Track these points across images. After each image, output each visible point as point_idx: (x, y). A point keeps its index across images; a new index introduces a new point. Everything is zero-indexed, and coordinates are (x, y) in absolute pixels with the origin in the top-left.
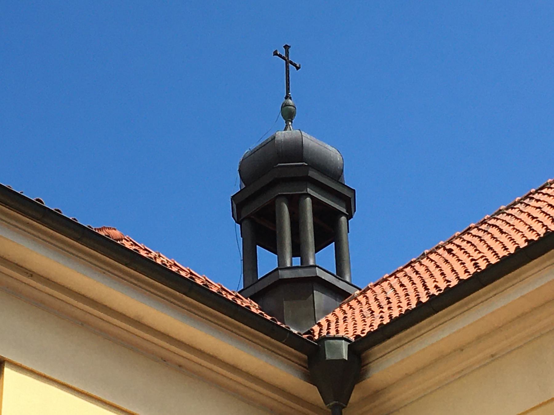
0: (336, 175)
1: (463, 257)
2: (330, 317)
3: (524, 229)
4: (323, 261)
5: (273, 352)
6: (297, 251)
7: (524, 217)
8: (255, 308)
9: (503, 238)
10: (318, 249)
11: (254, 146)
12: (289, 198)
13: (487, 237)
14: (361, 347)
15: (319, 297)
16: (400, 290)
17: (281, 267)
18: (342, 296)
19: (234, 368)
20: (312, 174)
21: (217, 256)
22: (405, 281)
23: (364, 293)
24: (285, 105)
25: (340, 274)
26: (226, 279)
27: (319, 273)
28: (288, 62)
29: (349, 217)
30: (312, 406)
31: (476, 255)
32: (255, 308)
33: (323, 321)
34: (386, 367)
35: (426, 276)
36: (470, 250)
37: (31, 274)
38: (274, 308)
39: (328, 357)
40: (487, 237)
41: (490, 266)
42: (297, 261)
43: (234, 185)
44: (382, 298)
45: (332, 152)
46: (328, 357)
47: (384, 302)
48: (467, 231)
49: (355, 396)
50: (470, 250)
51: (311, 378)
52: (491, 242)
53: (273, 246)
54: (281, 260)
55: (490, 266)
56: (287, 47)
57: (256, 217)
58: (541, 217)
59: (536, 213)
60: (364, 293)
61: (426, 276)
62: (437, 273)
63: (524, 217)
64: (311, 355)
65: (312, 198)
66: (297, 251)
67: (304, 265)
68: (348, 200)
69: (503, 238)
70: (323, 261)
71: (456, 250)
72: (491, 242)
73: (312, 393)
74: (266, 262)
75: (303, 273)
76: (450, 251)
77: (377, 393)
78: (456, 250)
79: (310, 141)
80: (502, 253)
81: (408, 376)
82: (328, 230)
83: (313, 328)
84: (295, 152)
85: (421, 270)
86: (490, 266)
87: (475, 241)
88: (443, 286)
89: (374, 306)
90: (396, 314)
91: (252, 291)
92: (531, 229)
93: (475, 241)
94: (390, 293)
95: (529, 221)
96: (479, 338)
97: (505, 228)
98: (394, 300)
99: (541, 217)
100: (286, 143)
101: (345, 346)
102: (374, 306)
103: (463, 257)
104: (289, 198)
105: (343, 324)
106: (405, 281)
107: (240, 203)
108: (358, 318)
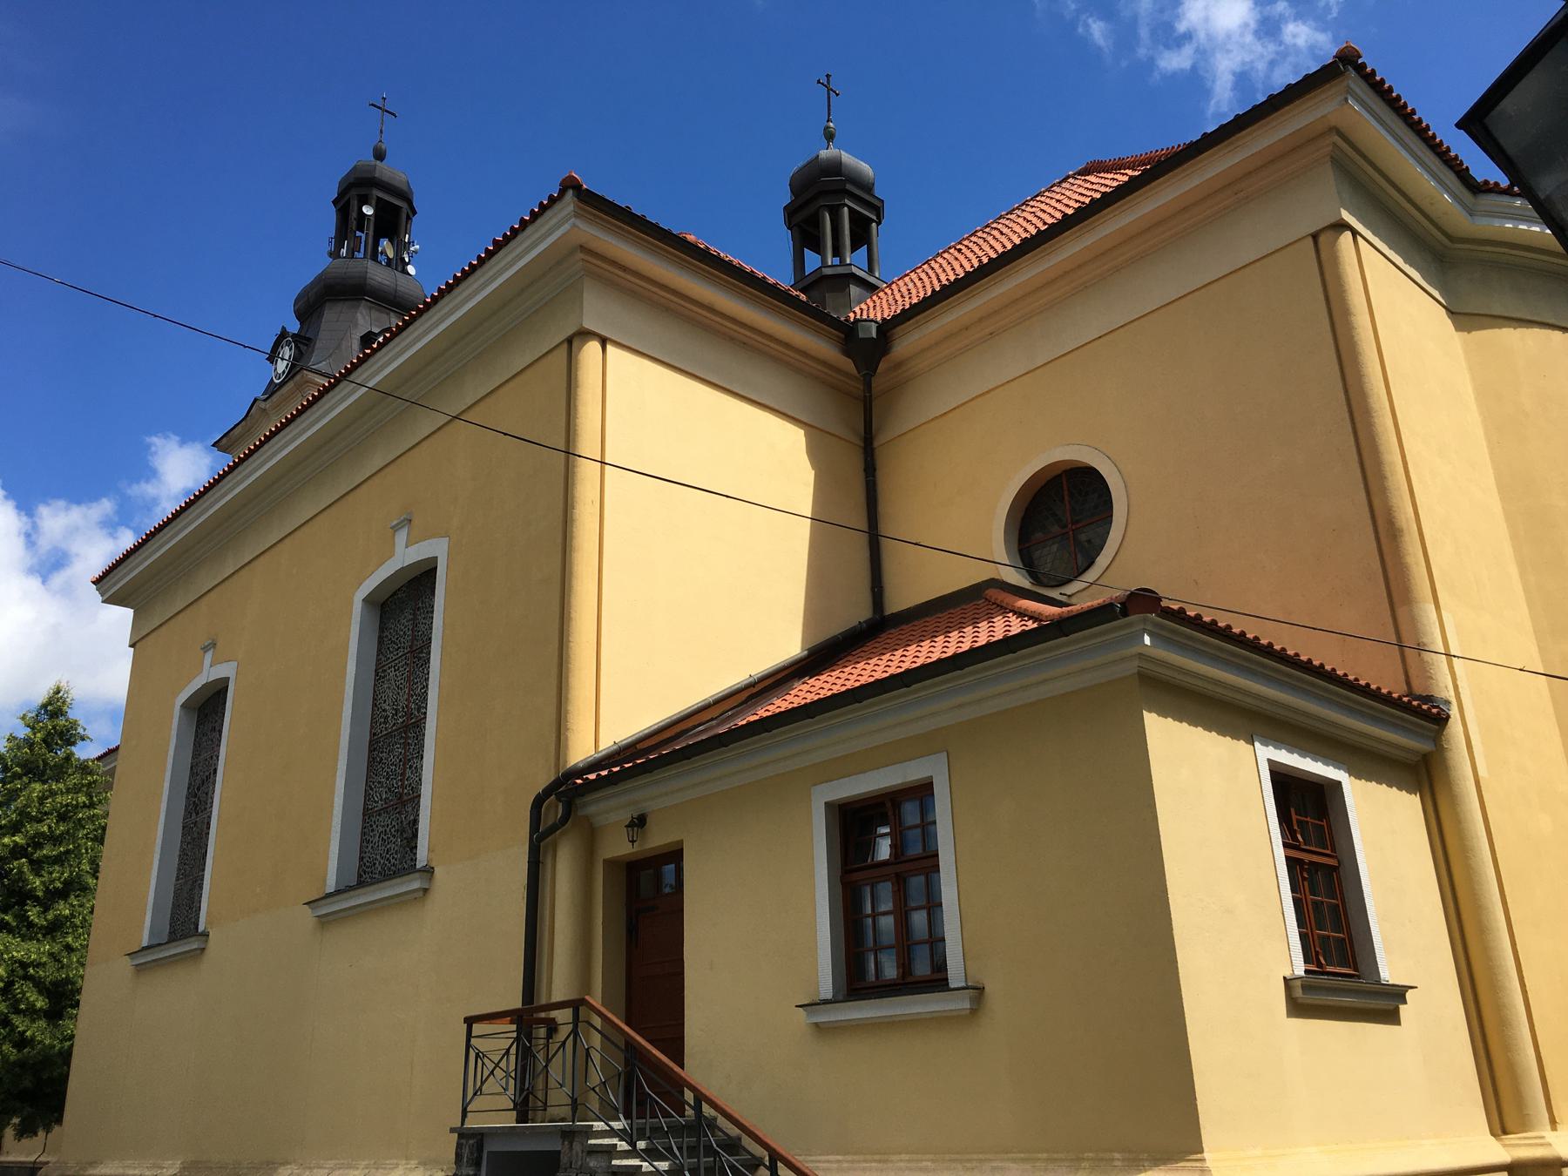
0: (868, 187)
1: (970, 255)
2: (863, 306)
3: (1020, 230)
4: (856, 260)
5: (817, 332)
6: (837, 251)
7: (1020, 220)
8: (803, 297)
9: (1003, 239)
10: (854, 249)
11: (801, 164)
12: (828, 206)
13: (990, 239)
14: (887, 328)
15: (854, 290)
16: (919, 284)
17: (824, 265)
18: (872, 289)
19: (787, 345)
20: (849, 187)
21: (773, 258)
22: (923, 276)
23: (889, 286)
24: (827, 128)
25: (871, 271)
26: (783, 278)
27: (854, 270)
28: (829, 90)
29: (879, 223)
30: (847, 374)
31: (980, 253)
32: (803, 297)
33: (857, 309)
34: (907, 343)
35: (939, 271)
36: (976, 249)
37: (625, 269)
38: (816, 299)
39: (861, 335)
40: (990, 239)
41: (967, 273)
42: (837, 261)
43: (786, 198)
44: (904, 289)
45: (865, 168)
46: (861, 335)
47: (906, 293)
48: (974, 234)
49: (882, 366)
50: (976, 249)
51: (847, 353)
52: (993, 242)
53: (818, 248)
54: (824, 260)
55: (967, 273)
56: (828, 76)
57: (805, 231)
58: (1035, 220)
59: (1030, 217)
60: (889, 286)
61: (939, 271)
62: (948, 269)
63: (1020, 220)
64: (847, 333)
65: (851, 210)
66: (837, 251)
67: (842, 263)
68: (878, 210)
69: (1003, 239)
70: (856, 260)
71: (964, 250)
72: (993, 242)
73: (848, 364)
74: (812, 261)
75: (841, 270)
76: (959, 251)
77: (899, 365)
78: (964, 250)
79: (846, 158)
80: (1000, 250)
81: (923, 351)
82: (861, 236)
83: (509, 1121)
84: (835, 167)
85: (936, 266)
86: (943, 287)
87: (981, 242)
88: (952, 278)
89: (898, 297)
90: (915, 301)
91: (801, 285)
92: (1026, 230)
93: (981, 242)
94: (911, 285)
95: (1024, 224)
96: (981, 320)
97: (1005, 230)
98: (914, 291)
99: (1035, 220)
100: (828, 160)
101: (874, 326)
102: (898, 297)
103: (970, 255)
104: (828, 206)
105: (873, 309)
106: (923, 276)
107: (791, 213)
108: (885, 306)
